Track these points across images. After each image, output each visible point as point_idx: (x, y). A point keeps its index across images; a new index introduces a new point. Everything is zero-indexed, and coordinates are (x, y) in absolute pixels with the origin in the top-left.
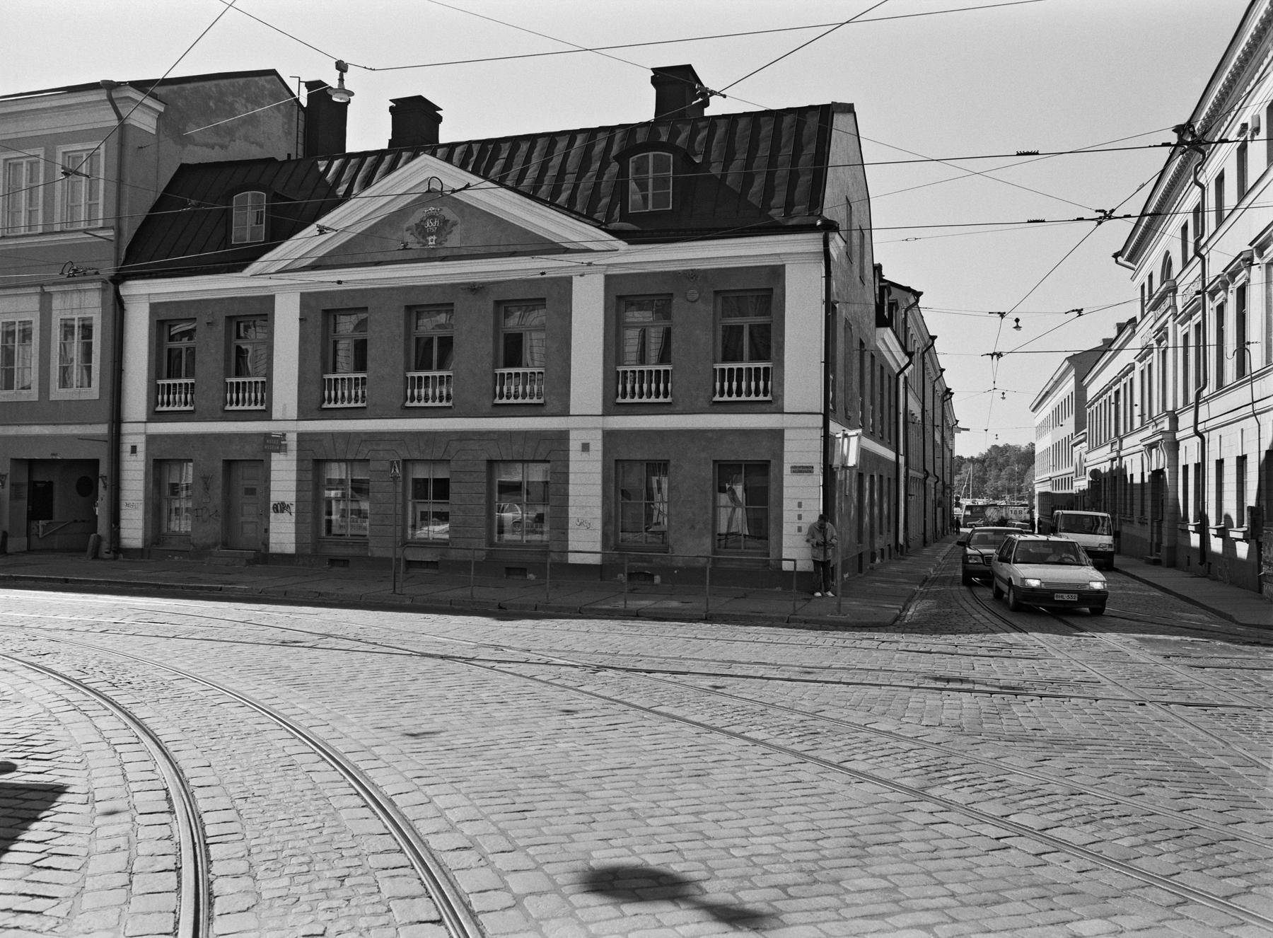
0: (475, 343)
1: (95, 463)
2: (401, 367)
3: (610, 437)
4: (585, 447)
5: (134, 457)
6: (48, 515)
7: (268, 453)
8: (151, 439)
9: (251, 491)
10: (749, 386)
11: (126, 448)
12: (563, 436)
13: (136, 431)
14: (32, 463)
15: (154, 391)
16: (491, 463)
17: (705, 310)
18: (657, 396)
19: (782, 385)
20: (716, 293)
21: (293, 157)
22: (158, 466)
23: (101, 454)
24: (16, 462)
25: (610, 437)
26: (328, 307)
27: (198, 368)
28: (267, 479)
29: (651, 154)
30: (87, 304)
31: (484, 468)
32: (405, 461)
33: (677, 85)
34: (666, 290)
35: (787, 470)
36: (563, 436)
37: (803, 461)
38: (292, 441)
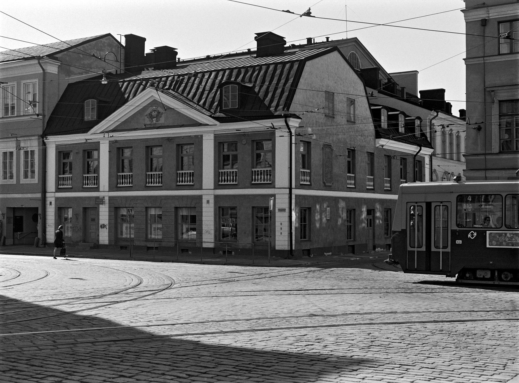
3: (216, 197)
4: (208, 202)
5: (51, 207)
8: (57, 199)
9: (93, 220)
10: (261, 178)
11: (48, 203)
12: (200, 197)
16: (176, 208)
17: (249, 147)
18: (225, 182)
20: (253, 141)
21: (118, 73)
23: (38, 205)
25: (216, 197)
27: (134, 169)
29: (230, 85)
30: (33, 145)
33: (309, 40)
36: (200, 197)
38: (107, 199)
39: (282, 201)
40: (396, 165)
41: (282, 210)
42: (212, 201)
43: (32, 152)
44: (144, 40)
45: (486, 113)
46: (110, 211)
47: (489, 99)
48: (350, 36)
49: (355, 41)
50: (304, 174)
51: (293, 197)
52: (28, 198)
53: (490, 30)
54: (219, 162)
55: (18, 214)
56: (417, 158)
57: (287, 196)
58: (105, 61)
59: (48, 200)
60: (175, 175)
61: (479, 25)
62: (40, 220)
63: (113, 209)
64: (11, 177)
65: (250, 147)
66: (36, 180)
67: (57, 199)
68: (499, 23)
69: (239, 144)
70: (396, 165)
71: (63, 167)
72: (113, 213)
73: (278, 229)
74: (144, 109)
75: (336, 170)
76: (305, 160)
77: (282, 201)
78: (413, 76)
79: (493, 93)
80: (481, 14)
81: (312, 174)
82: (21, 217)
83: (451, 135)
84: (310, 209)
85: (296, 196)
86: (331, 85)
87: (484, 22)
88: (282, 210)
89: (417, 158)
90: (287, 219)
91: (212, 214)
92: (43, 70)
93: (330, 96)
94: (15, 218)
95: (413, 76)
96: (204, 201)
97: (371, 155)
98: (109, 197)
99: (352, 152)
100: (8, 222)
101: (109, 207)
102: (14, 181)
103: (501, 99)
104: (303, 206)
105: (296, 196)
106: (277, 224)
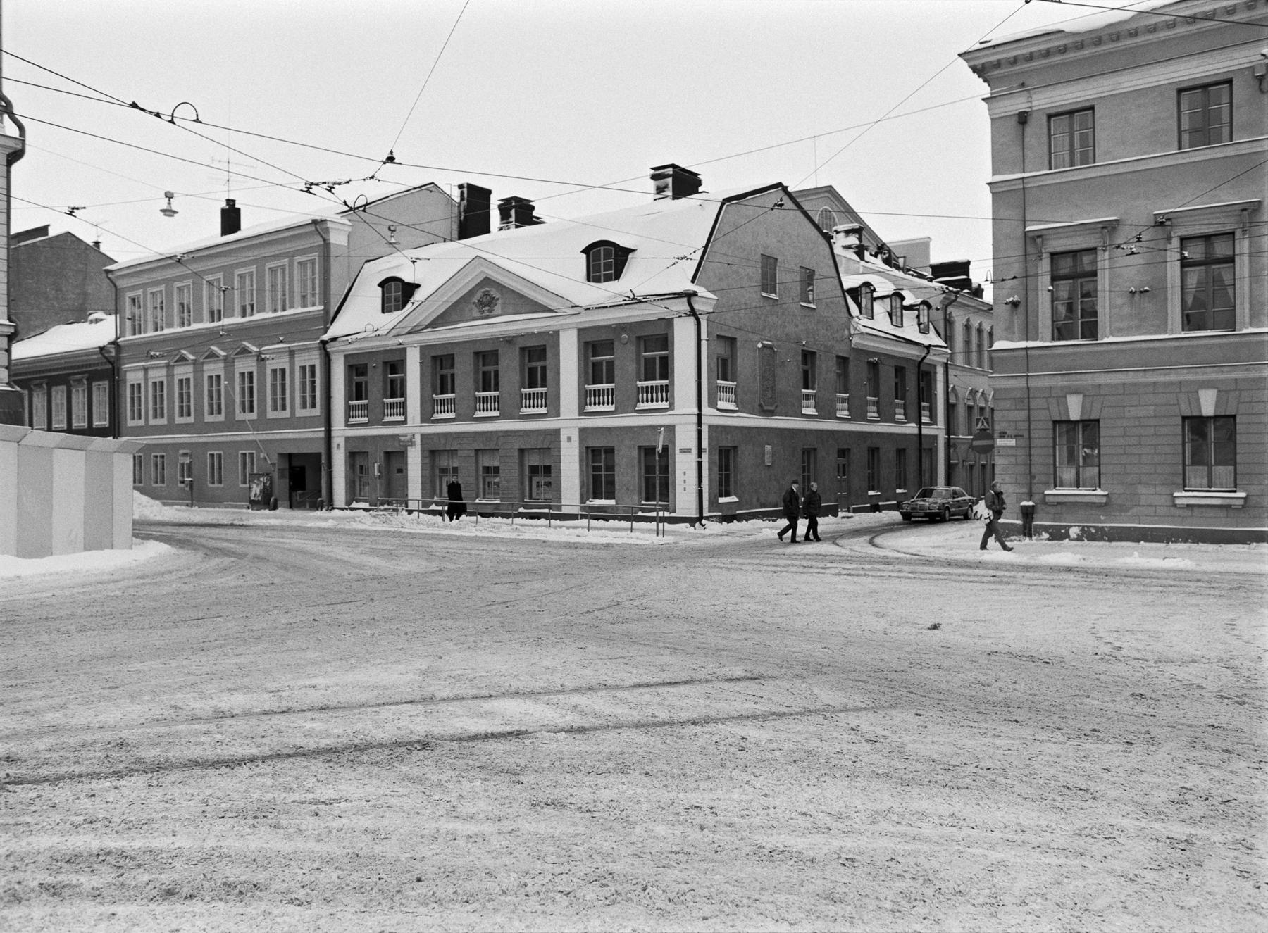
0: (510, 368)
1: (319, 454)
2: (517, 385)
3: (583, 431)
4: (569, 439)
6: (303, 488)
7: (406, 447)
8: (348, 439)
9: (400, 471)
12: (556, 432)
13: (340, 432)
14: (290, 456)
15: (349, 409)
16: (521, 451)
17: (632, 349)
19: (559, 477)
20: (639, 338)
22: (352, 456)
23: (321, 449)
24: (281, 455)
25: (583, 431)
26: (434, 354)
27: (457, 389)
28: (406, 464)
31: (516, 453)
32: (477, 451)
34: (611, 337)
35: (677, 451)
36: (556, 432)
37: (684, 456)
38: (418, 439)
39: (685, 437)
40: (887, 375)
41: (686, 451)
42: (575, 438)
43: (313, 367)
44: (489, 192)
45: (1027, 277)
46: (423, 457)
47: (1031, 250)
48: (822, 183)
49: (830, 190)
50: (725, 389)
51: (705, 429)
52: (306, 437)
53: (1036, 127)
54: (586, 373)
55: (296, 463)
56: (923, 368)
57: (694, 428)
58: (172, 121)
59: (335, 441)
60: (518, 397)
61: (1014, 121)
62: (323, 473)
63: (427, 454)
64: (284, 408)
65: (634, 348)
66: (317, 411)
67: (348, 439)
68: (1050, 117)
69: (616, 343)
70: (887, 375)
71: (356, 391)
72: (427, 460)
73: (679, 481)
74: (471, 293)
75: (781, 385)
76: (724, 368)
77: (685, 437)
78: (924, 245)
79: (1039, 240)
80: (1019, 104)
81: (739, 390)
82: (303, 469)
83: (980, 331)
84: (735, 448)
85: (710, 426)
86: (771, 244)
87: (1023, 118)
88: (686, 451)
89: (923, 368)
90: (694, 466)
91: (577, 459)
92: (324, 240)
93: (769, 264)
94: (291, 468)
95: (924, 245)
96: (563, 438)
97: (843, 361)
98: (422, 436)
99: (808, 357)
100: (282, 476)
101: (423, 451)
102: (287, 414)
103: (1052, 250)
104: (724, 443)
105: (710, 426)
106: (679, 474)
